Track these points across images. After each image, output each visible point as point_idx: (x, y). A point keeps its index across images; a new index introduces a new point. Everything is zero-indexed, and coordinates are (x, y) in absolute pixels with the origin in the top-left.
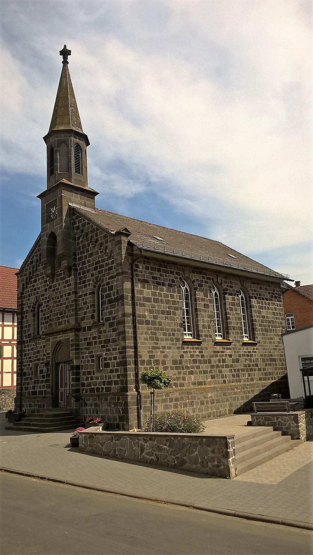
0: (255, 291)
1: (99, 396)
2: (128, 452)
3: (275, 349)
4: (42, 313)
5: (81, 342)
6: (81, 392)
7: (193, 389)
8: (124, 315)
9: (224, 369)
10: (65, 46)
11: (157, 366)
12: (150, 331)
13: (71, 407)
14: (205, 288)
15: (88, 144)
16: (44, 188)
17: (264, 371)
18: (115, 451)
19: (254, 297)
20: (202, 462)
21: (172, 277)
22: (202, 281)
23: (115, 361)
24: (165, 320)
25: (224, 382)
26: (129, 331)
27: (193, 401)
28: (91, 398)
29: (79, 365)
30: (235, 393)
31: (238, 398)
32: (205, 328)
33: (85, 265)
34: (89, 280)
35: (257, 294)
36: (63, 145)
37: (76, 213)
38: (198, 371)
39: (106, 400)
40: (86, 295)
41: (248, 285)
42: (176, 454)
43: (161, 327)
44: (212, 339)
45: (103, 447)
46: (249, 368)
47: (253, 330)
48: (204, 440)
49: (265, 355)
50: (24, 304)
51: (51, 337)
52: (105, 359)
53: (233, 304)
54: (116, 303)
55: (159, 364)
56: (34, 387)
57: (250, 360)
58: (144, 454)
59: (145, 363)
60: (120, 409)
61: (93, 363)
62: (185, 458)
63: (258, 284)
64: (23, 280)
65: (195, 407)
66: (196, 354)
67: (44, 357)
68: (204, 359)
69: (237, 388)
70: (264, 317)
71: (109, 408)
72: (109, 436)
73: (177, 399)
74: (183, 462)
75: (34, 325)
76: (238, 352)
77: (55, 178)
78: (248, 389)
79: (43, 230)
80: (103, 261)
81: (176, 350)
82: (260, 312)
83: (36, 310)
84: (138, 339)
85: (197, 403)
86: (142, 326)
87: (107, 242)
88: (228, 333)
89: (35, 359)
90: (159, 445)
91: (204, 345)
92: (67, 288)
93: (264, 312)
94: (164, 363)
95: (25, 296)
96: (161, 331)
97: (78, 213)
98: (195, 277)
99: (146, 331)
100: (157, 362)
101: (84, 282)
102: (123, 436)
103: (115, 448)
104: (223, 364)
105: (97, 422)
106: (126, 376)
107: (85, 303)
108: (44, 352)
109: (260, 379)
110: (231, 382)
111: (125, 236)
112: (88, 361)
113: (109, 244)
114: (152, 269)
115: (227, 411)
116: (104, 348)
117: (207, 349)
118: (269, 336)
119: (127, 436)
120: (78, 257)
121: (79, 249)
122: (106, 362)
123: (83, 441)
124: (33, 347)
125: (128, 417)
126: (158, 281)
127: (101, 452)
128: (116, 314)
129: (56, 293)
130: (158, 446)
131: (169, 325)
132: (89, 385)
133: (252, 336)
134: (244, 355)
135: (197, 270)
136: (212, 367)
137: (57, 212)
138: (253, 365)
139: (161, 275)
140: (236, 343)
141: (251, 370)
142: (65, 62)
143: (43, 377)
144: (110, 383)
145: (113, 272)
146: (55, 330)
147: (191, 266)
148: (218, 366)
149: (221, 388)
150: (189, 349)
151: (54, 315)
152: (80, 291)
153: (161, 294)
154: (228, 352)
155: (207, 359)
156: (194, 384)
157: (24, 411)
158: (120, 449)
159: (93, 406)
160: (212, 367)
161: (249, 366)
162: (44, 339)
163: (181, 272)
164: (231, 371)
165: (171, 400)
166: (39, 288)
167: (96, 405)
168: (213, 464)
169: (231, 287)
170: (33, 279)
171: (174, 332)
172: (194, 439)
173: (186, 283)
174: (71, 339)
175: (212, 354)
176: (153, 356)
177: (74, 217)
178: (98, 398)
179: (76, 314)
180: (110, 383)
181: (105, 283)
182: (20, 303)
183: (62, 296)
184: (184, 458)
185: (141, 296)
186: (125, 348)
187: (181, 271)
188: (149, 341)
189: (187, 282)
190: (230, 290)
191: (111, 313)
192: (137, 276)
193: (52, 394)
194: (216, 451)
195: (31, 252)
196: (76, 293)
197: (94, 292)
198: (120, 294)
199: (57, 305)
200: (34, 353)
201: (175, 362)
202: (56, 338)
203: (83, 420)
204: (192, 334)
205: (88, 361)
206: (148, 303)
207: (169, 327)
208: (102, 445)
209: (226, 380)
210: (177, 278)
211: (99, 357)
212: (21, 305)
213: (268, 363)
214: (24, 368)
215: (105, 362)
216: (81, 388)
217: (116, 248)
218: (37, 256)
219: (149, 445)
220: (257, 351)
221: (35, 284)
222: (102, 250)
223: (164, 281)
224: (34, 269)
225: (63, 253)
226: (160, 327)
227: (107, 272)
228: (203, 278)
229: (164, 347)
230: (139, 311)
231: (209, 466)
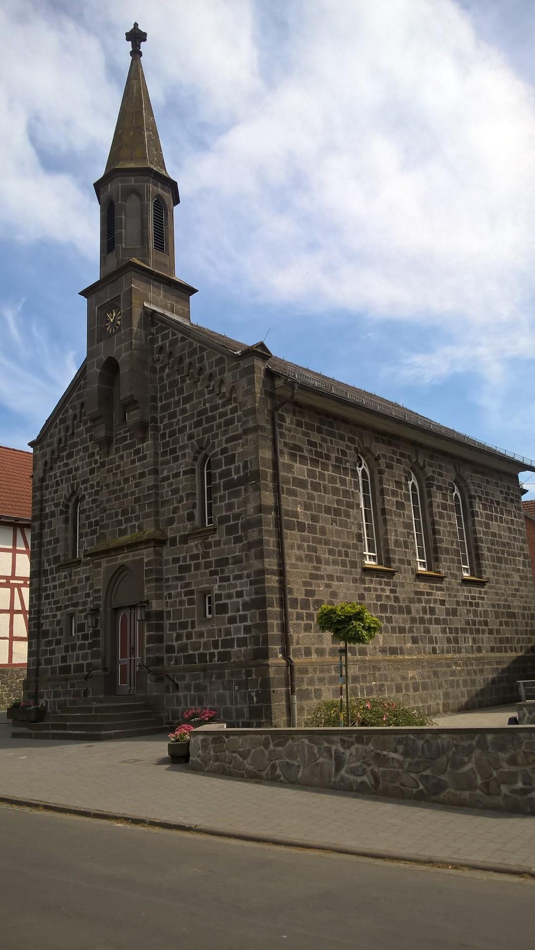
0: (480, 486)
1: (204, 670)
2: (305, 770)
3: (514, 595)
4: (83, 516)
5: (165, 565)
6: (166, 665)
8: (260, 509)
9: (433, 627)
12: (305, 544)
13: (146, 692)
14: (397, 472)
15: (177, 201)
16: (93, 276)
17: (497, 634)
18: (274, 767)
20: (487, 784)
21: (342, 445)
22: (392, 459)
23: (240, 600)
24: (332, 525)
25: (434, 651)
26: (271, 541)
27: (383, 685)
28: (187, 675)
29: (162, 612)
30: (453, 673)
31: (458, 682)
32: (398, 547)
33: (174, 418)
34: (183, 448)
37: (157, 322)
38: (390, 628)
40: (177, 475)
42: (421, 770)
44: (412, 569)
45: (245, 761)
46: (472, 627)
47: (478, 557)
48: (490, 737)
49: (499, 606)
50: (47, 501)
51: (102, 560)
52: (219, 597)
53: (444, 507)
54: (243, 487)
56: (64, 659)
57: (475, 613)
58: (343, 772)
59: (298, 604)
60: (253, 694)
61: (191, 606)
62: (444, 777)
63: (483, 474)
64: (44, 455)
65: (387, 696)
67: (87, 599)
68: (399, 604)
69: (456, 664)
70: (494, 535)
71: (227, 693)
72: (259, 736)
74: (440, 787)
77: (117, 256)
78: (474, 667)
79: (91, 353)
80: (214, 408)
81: (352, 584)
82: (487, 526)
83: (70, 510)
84: (287, 558)
85: (390, 689)
86: (292, 532)
87: (222, 371)
88: (437, 559)
89: (69, 604)
90: (379, 751)
91: (398, 578)
92: (137, 464)
93: (494, 525)
95: (48, 484)
96: (324, 544)
97: (163, 321)
98: (379, 449)
99: (299, 542)
101: (173, 451)
102: (293, 736)
103: (274, 762)
104: (431, 617)
105: (207, 719)
106: (264, 627)
107: (175, 491)
108: (86, 590)
109: (492, 650)
110: (445, 652)
111: (261, 359)
112: (182, 603)
114: (308, 426)
115: (441, 707)
116: (215, 576)
117: (403, 586)
118: (504, 571)
119: (301, 736)
120: (159, 404)
121: (163, 389)
122: (220, 602)
123: (200, 750)
124: (63, 581)
125: (269, 709)
126: (318, 450)
127: (243, 770)
128: (241, 509)
129: (115, 475)
130: (378, 755)
131: (339, 536)
132: (183, 648)
133: (477, 567)
134: (465, 603)
135: (384, 438)
136: (413, 620)
137: (120, 320)
138: (480, 623)
139: (323, 440)
140: (451, 579)
141: (478, 631)
142: (136, 53)
143: (85, 637)
144: (228, 643)
145: (237, 428)
146: (112, 545)
149: (430, 663)
150: (372, 583)
151: (110, 516)
152: (165, 469)
153: (323, 475)
154: (439, 595)
155: (404, 605)
156: (383, 651)
157: (44, 705)
158: (287, 763)
159: (192, 690)
160: (413, 620)
162: (87, 564)
166: (77, 469)
167: (198, 688)
168: (514, 787)
169: (440, 475)
170: (66, 453)
171: (347, 549)
172: (464, 736)
173: (363, 461)
175: (412, 595)
177: (153, 330)
178: (202, 674)
180: (228, 643)
181: (218, 451)
182: (38, 498)
183: (127, 480)
184: (442, 778)
185: (290, 475)
186: (262, 572)
188: (305, 563)
189: (366, 458)
190: (438, 480)
191: (230, 507)
192: (281, 437)
193: (105, 669)
194: (519, 760)
195: (63, 400)
196: (156, 472)
198: (251, 468)
199: (118, 498)
200: (66, 593)
203: (169, 719)
204: (375, 556)
205: (182, 603)
207: (339, 540)
208: (244, 755)
209: (437, 648)
211: (204, 593)
212: (39, 503)
213: (503, 620)
214: (43, 623)
215: (217, 602)
216: (165, 656)
217: (244, 382)
218: (74, 408)
219: (354, 754)
220: (485, 596)
221: (70, 461)
222: (211, 388)
223: (328, 451)
224: (69, 434)
226: (323, 537)
228: (394, 453)
229: (330, 577)
230: (288, 501)
231: (502, 793)
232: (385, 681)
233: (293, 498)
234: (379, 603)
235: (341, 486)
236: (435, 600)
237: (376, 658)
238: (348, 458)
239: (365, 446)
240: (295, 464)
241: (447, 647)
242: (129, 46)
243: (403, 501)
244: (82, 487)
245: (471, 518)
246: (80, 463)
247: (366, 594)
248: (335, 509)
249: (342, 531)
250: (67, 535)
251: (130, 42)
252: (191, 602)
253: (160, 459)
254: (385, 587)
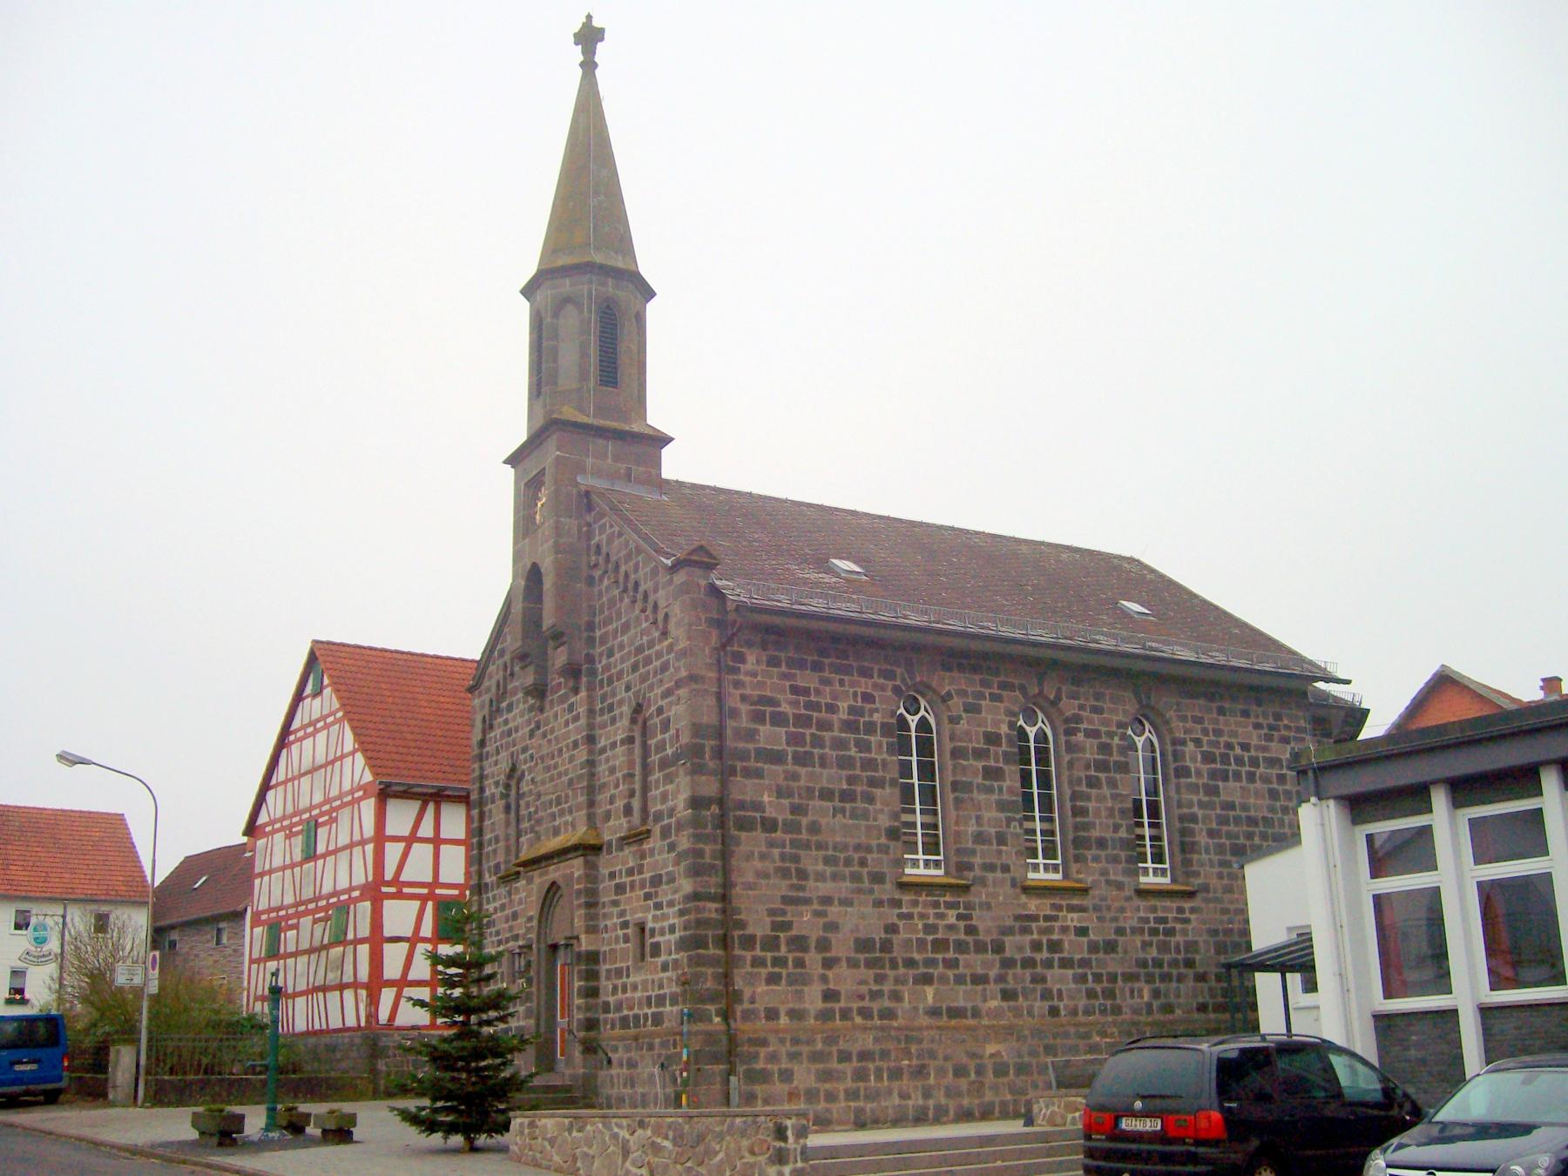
7: (930, 1028)
10: (589, 17)
19: (1191, 740)
21: (865, 685)
25: (1054, 1012)
34: (621, 703)
35: (1205, 732)
36: (570, 308)
39: (651, 1047)
40: (614, 745)
41: (1166, 702)
55: (805, 949)
66: (944, 922)
70: (1230, 806)
73: (864, 1056)
75: (507, 839)
76: (1115, 919)
80: (651, 644)
91: (979, 895)
94: (824, 945)
99: (764, 849)
100: (799, 943)
101: (611, 708)
114: (791, 663)
141: (1166, 978)
142: (589, 66)
144: (661, 1000)
147: (939, 650)
148: (1029, 963)
150: (921, 906)
153: (821, 739)
154: (1073, 920)
156: (934, 1012)
160: (1008, 963)
161: (1158, 963)
164: (1082, 979)
165: (845, 1057)
169: (1096, 710)
176: (787, 926)
177: (589, 518)
179: (591, 804)
190: (1091, 722)
196: (591, 739)
197: (633, 737)
201: (864, 945)
210: (883, 688)
216: (602, 1017)
221: (510, 716)
223: (835, 698)
225: (553, 626)
227: (659, 677)
229: (827, 901)
233: (757, 781)
238: (878, 705)
239: (918, 679)
240: (761, 728)
242: (577, 54)
243: (1001, 765)
244: (522, 757)
247: (901, 924)
249: (857, 827)
250: (509, 831)
251: (580, 47)
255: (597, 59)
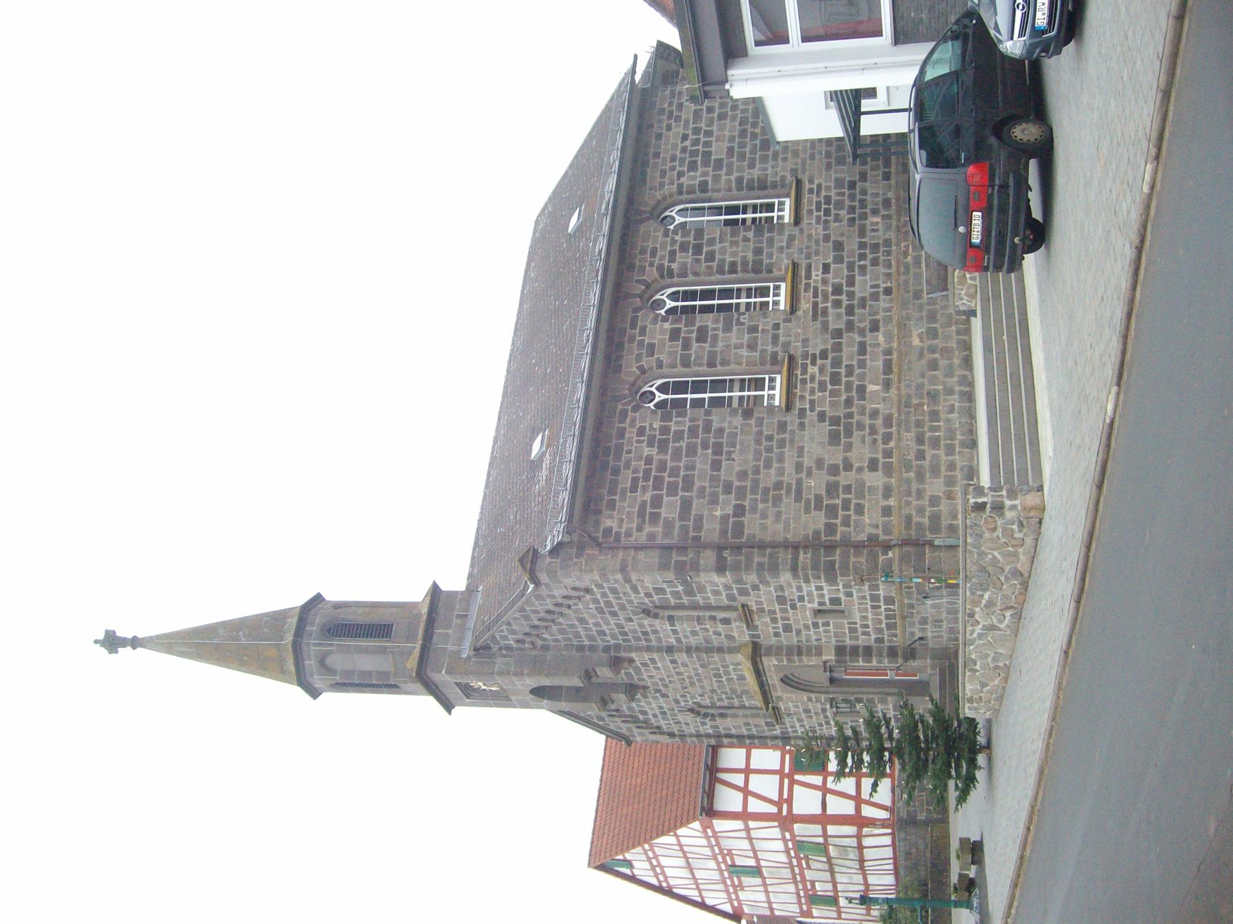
0: (663, 173)
10: (96, 642)
11: (841, 488)
12: (760, 506)
14: (658, 337)
19: (678, 179)
21: (631, 433)
25: (888, 291)
39: (911, 606)
40: (675, 632)
43: (750, 472)
55: (837, 484)
63: (645, 164)
66: (817, 375)
73: (920, 440)
74: (1016, 573)
76: (817, 242)
80: (596, 601)
91: (797, 348)
94: (834, 470)
98: (630, 368)
107: (694, 633)
113: (556, 593)
114: (612, 492)
129: (670, 682)
136: (850, 326)
138: (852, 197)
141: (863, 204)
142: (135, 643)
144: (875, 598)
148: (850, 310)
153: (672, 469)
154: (817, 275)
156: (887, 385)
160: (850, 326)
163: (620, 407)
164: (863, 269)
165: (921, 455)
174: (776, 663)
177: (495, 648)
179: (720, 650)
183: (678, 674)
187: (616, 407)
190: (663, 258)
194: (992, 526)
196: (670, 650)
199: (700, 681)
201: (834, 438)
202: (774, 686)
206: (694, 506)
210: (633, 420)
216: (887, 644)
220: (816, 182)
221: (650, 713)
223: (641, 458)
229: (799, 467)
232: (923, 389)
234: (829, 387)
235: (683, 439)
236: (825, 282)
237: (895, 399)
238: (647, 424)
239: (627, 392)
241: (884, 266)
242: (125, 652)
243: (696, 328)
244: (683, 704)
245: (710, 193)
246: (654, 705)
248: (715, 453)
250: (741, 714)
251: (119, 649)
252: (827, 624)
253: (654, 643)
254: (809, 374)
255: (130, 636)
